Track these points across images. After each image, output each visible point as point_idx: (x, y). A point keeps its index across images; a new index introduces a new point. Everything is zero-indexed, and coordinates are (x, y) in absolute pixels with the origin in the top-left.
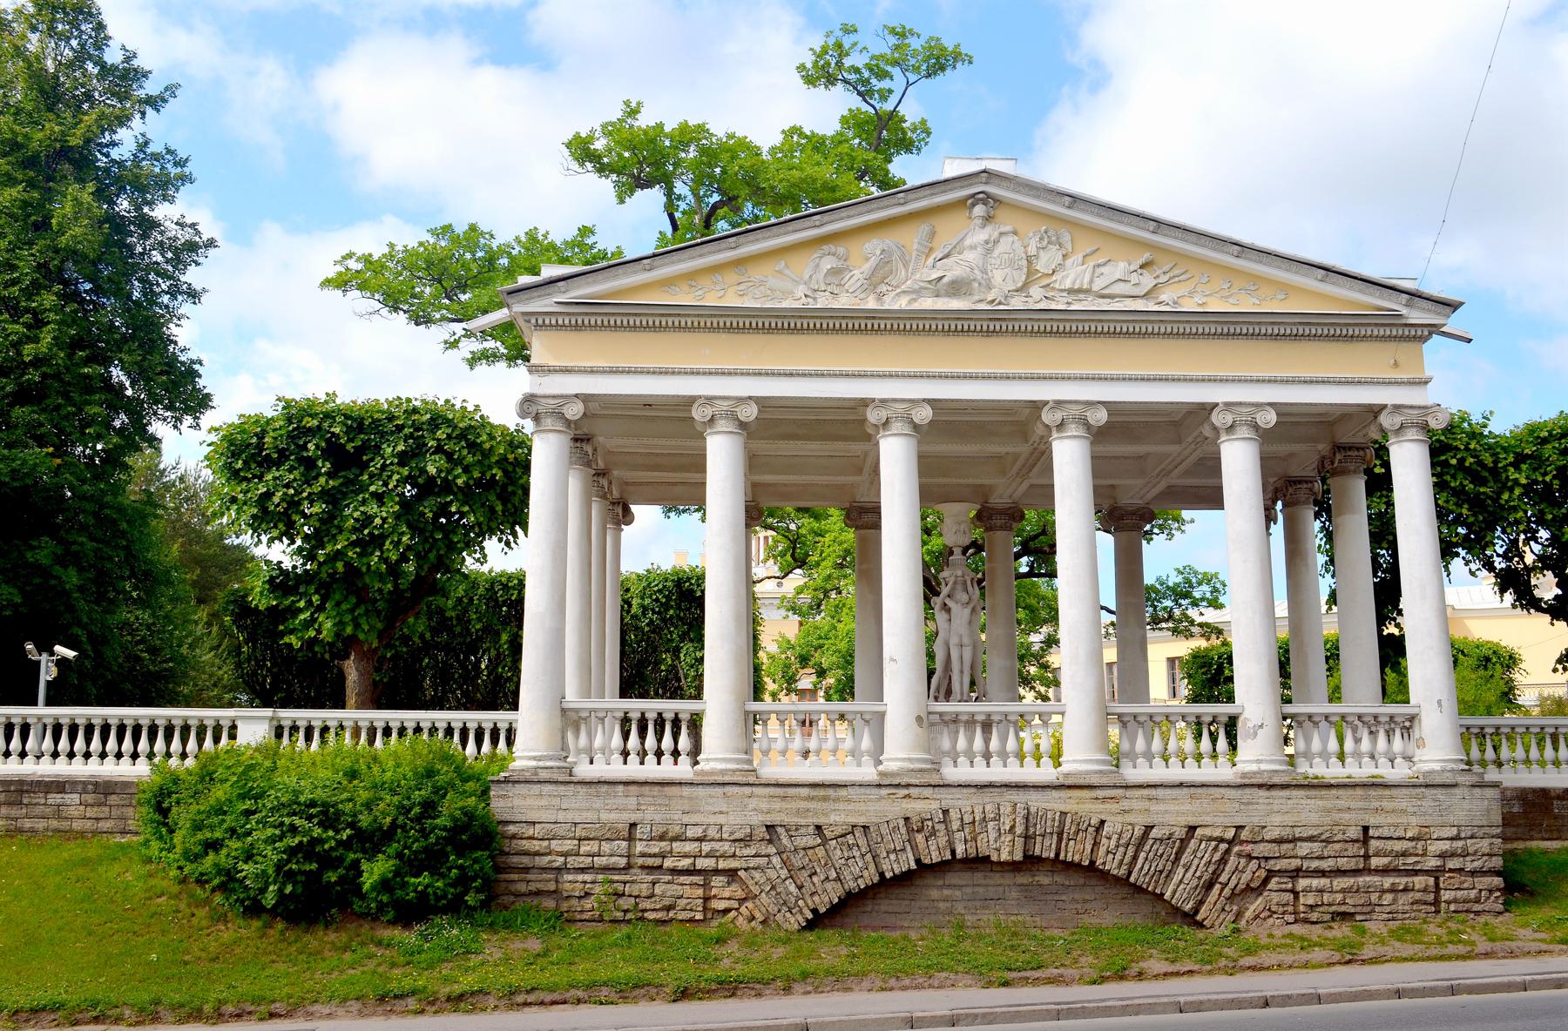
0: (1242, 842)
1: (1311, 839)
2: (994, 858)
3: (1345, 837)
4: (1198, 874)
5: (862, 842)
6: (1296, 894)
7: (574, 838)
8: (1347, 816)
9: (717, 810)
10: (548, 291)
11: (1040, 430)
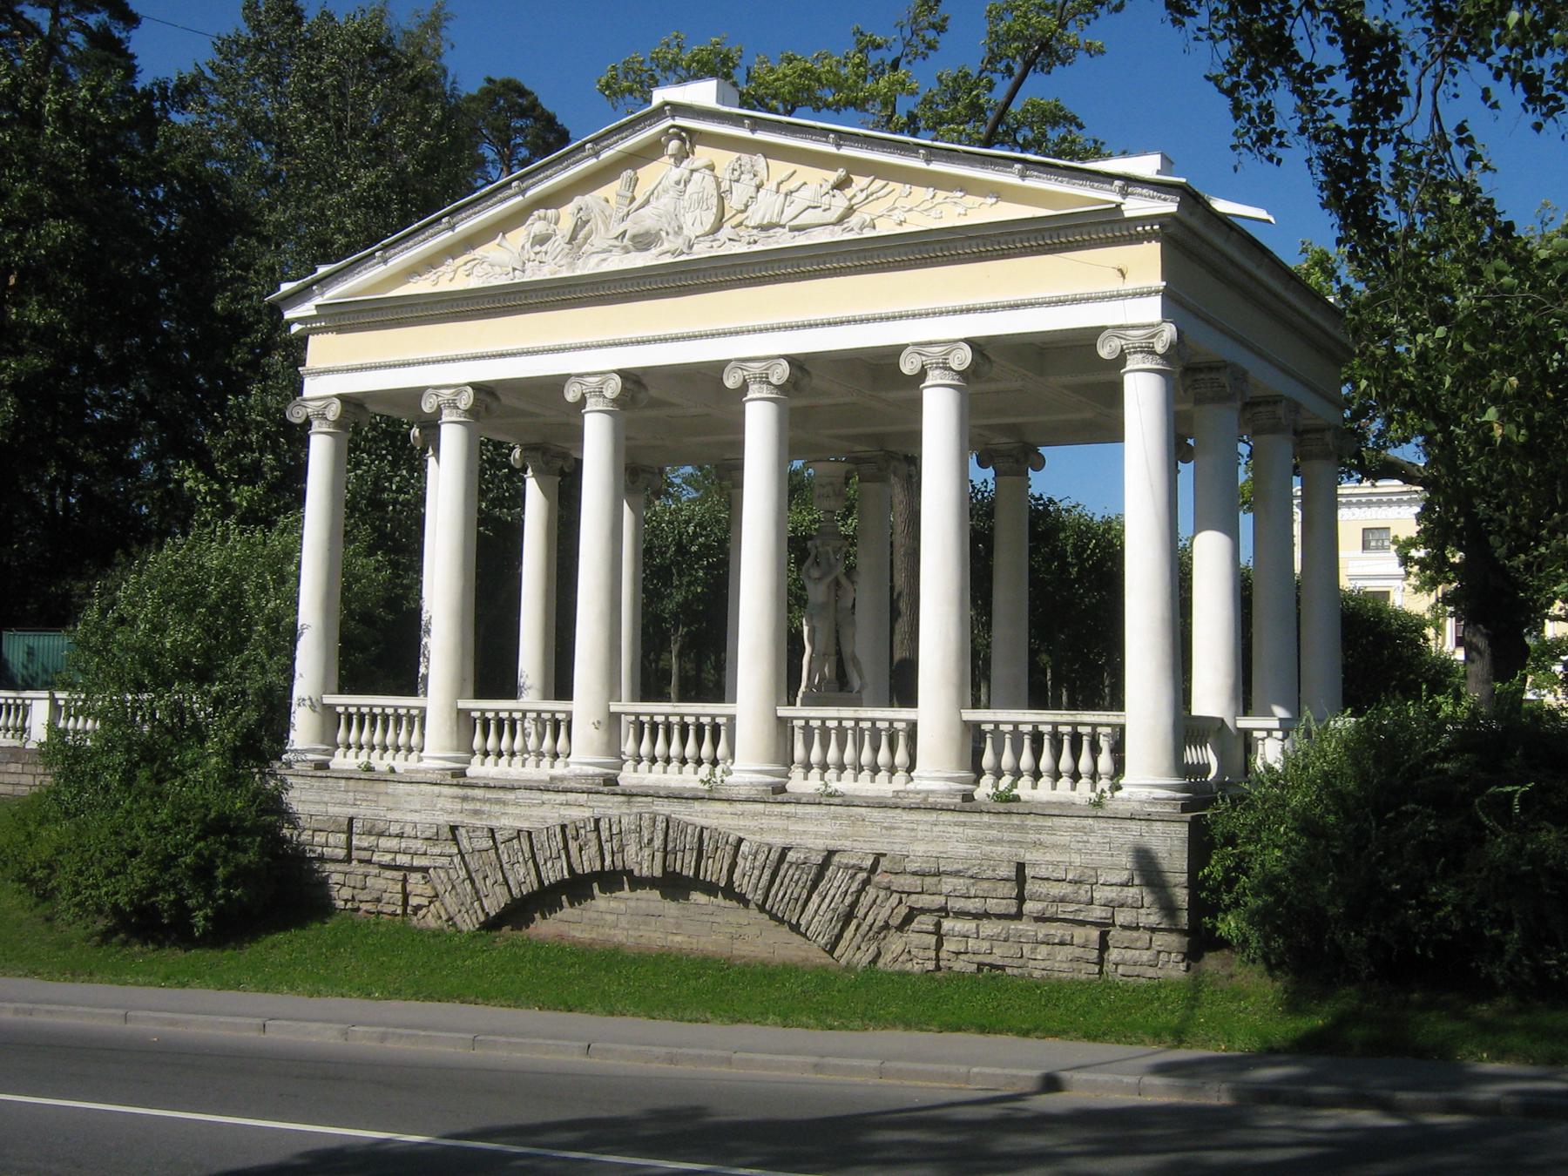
1: (957, 874)
3: (994, 875)
8: (999, 849)
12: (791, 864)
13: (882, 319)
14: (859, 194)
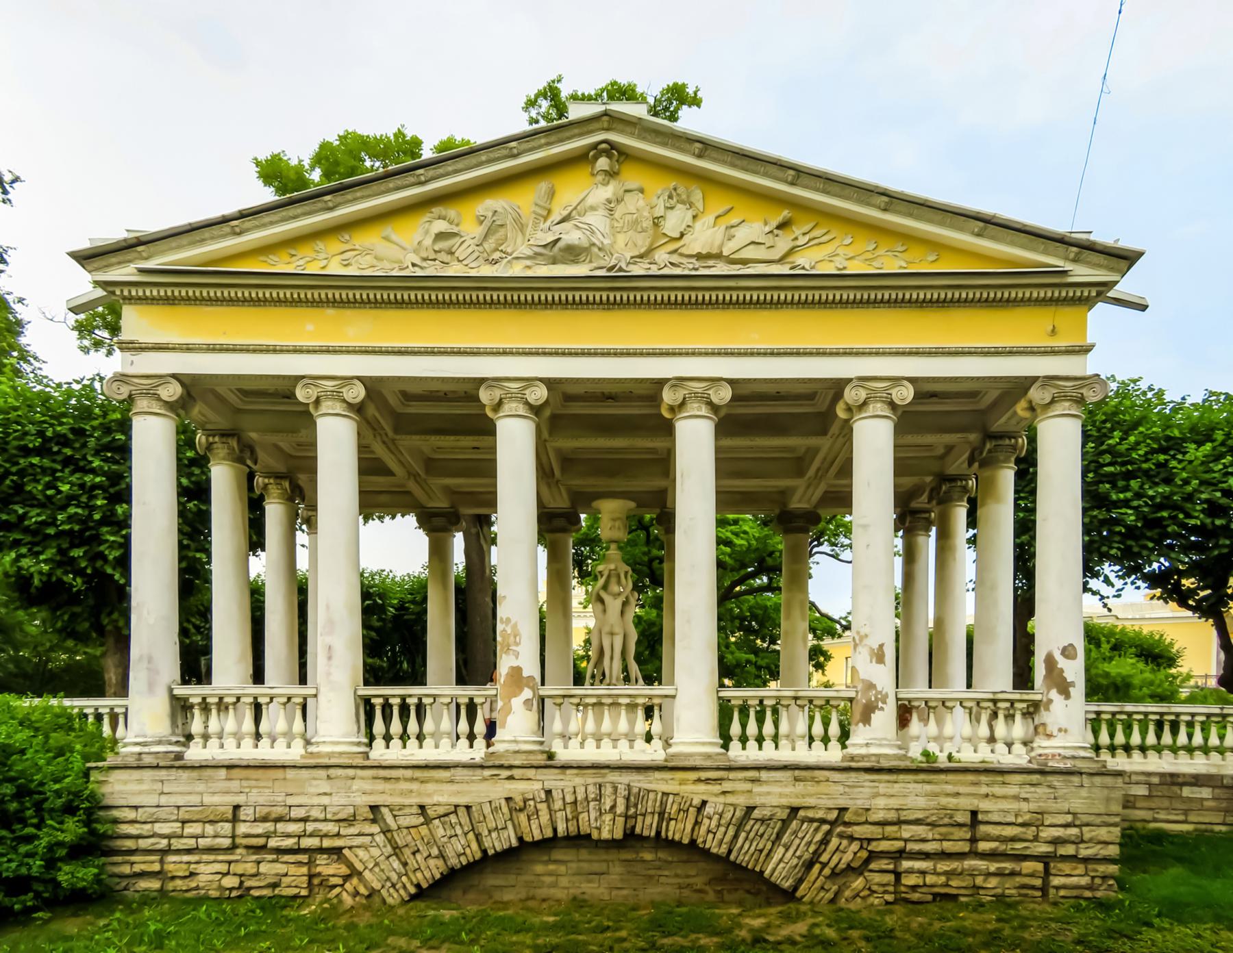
1: (917, 822)
2: (595, 836)
4: (798, 853)
5: (464, 819)
6: (898, 875)
7: (177, 821)
12: (757, 820)
14: (800, 237)
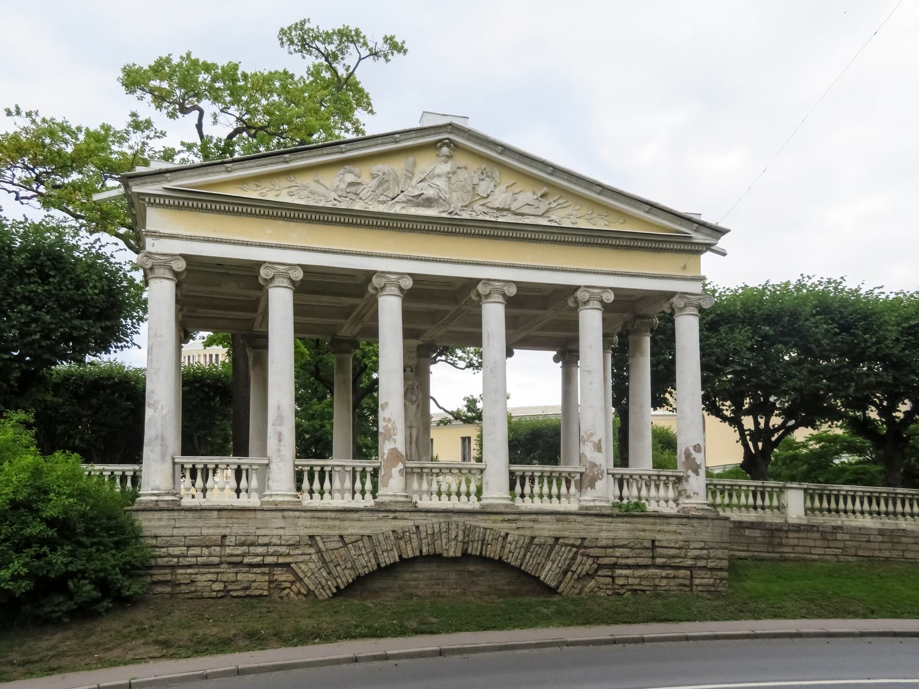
0: (586, 548)
1: (623, 546)
4: (560, 565)
6: (613, 578)
7: (184, 546)
9: (279, 526)
10: (157, 179)
11: (371, 290)
13: (594, 273)
